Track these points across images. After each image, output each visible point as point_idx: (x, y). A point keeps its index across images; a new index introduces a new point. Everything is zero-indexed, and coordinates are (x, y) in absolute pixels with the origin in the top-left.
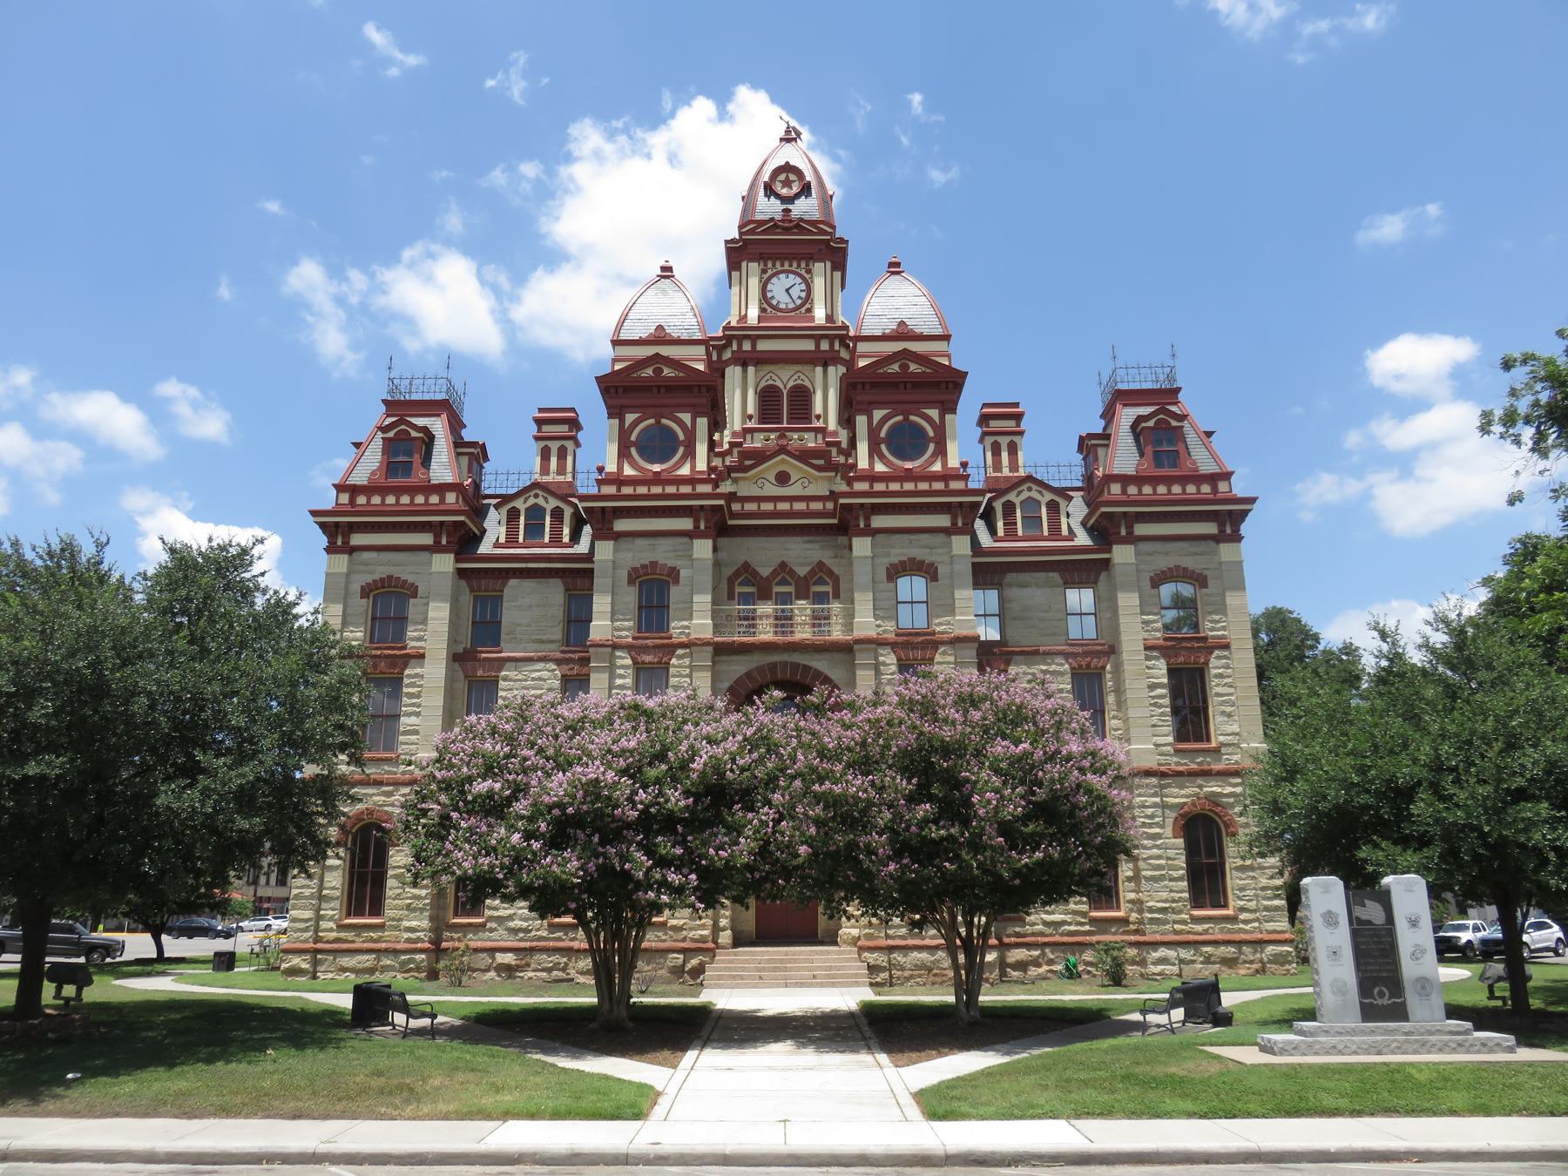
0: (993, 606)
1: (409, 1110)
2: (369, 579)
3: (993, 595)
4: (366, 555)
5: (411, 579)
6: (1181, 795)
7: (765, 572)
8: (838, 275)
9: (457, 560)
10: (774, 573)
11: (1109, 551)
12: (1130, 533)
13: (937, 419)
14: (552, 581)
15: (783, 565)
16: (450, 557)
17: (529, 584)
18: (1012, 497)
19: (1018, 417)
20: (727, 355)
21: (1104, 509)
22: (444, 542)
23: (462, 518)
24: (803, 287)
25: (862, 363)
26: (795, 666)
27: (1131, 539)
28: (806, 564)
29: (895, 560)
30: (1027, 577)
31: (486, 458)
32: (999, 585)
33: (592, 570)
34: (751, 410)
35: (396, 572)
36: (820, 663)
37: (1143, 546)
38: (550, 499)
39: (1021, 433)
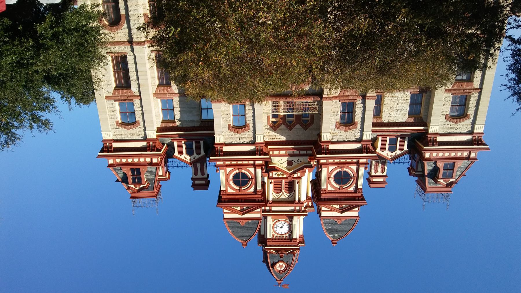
0: (204, 113)
1: (119, 55)
3: (204, 117)
7: (298, 126)
8: (262, 233)
10: (294, 125)
13: (228, 187)
15: (306, 129)
18: (197, 157)
20: (305, 204)
23: (425, 148)
25: (258, 210)
30: (191, 125)
31: (409, 169)
32: (203, 121)
33: (373, 126)
34: (297, 185)
35: (454, 125)
38: (385, 155)
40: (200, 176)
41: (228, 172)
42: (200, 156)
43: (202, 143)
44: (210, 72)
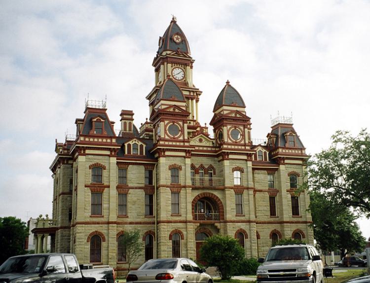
2: (91, 164)
3: (272, 176)
4: (90, 156)
5: (103, 164)
6: (93, 229)
9: (117, 159)
11: (279, 166)
12: (84, 152)
14: (141, 166)
15: (202, 165)
16: (115, 158)
17: (135, 166)
18: (130, 142)
19: (133, 114)
21: (158, 147)
22: (113, 154)
24: (183, 73)
26: (207, 193)
27: (284, 164)
28: (207, 165)
29: (234, 167)
36: (216, 193)
37: (286, 165)
39: (133, 120)
40: (128, 122)
41: (166, 123)
42: (128, 143)
43: (126, 153)
44: (202, 229)
